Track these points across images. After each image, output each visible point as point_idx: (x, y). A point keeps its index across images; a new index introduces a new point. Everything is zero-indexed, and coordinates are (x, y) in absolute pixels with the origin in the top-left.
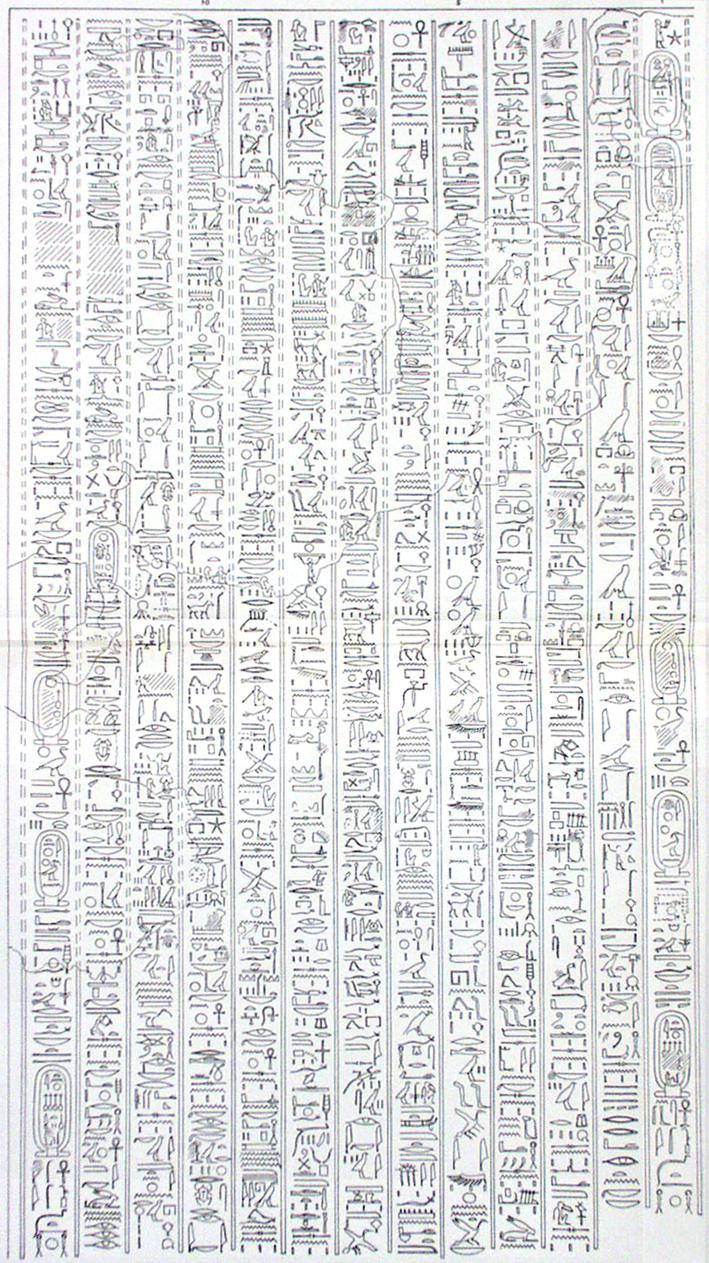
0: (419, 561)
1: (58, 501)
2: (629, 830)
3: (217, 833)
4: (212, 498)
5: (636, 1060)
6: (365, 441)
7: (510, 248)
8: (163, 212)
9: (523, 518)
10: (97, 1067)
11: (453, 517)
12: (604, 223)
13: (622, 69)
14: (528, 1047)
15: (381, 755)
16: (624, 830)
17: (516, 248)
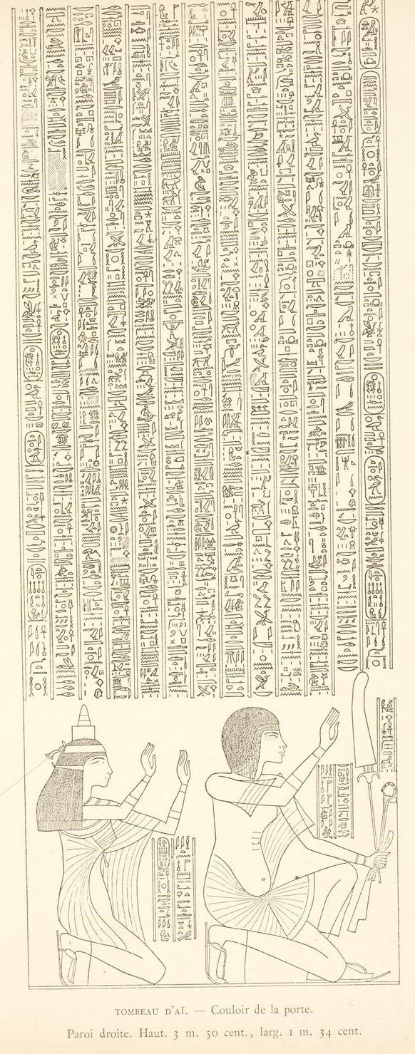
0: (233, 280)
1: (33, 240)
2: (352, 448)
3: (124, 504)
4: (120, 317)
5: (354, 590)
6: (203, 254)
7: (284, 134)
8: (89, 135)
9: (291, 272)
10: (61, 592)
11: (253, 285)
12: (338, 119)
13: (347, 31)
14: (295, 580)
15: (214, 432)
16: (349, 448)
17: (287, 133)
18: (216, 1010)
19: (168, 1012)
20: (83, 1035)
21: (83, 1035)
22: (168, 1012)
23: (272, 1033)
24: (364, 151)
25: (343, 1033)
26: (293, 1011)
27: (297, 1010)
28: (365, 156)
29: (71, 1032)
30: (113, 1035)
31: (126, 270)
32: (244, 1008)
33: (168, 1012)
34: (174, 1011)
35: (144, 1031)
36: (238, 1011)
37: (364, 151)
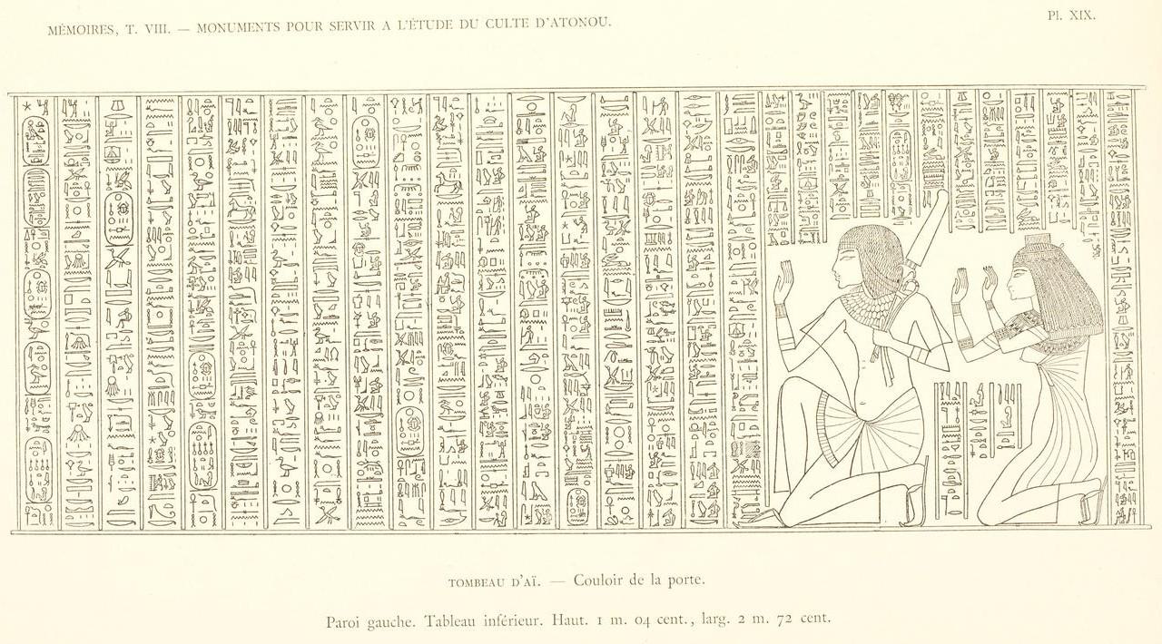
18: (580, 580)
19: (515, 583)
20: (346, 624)
21: (346, 624)
22: (516, 582)
23: (717, 620)
24: (190, 159)
25: (663, 621)
26: (680, 581)
27: (684, 580)
28: (193, 164)
29: (331, 620)
30: (352, 624)
31: (268, 112)
32: (617, 578)
33: (516, 582)
34: (523, 581)
35: (558, 617)
36: (609, 582)
37: (190, 159)
